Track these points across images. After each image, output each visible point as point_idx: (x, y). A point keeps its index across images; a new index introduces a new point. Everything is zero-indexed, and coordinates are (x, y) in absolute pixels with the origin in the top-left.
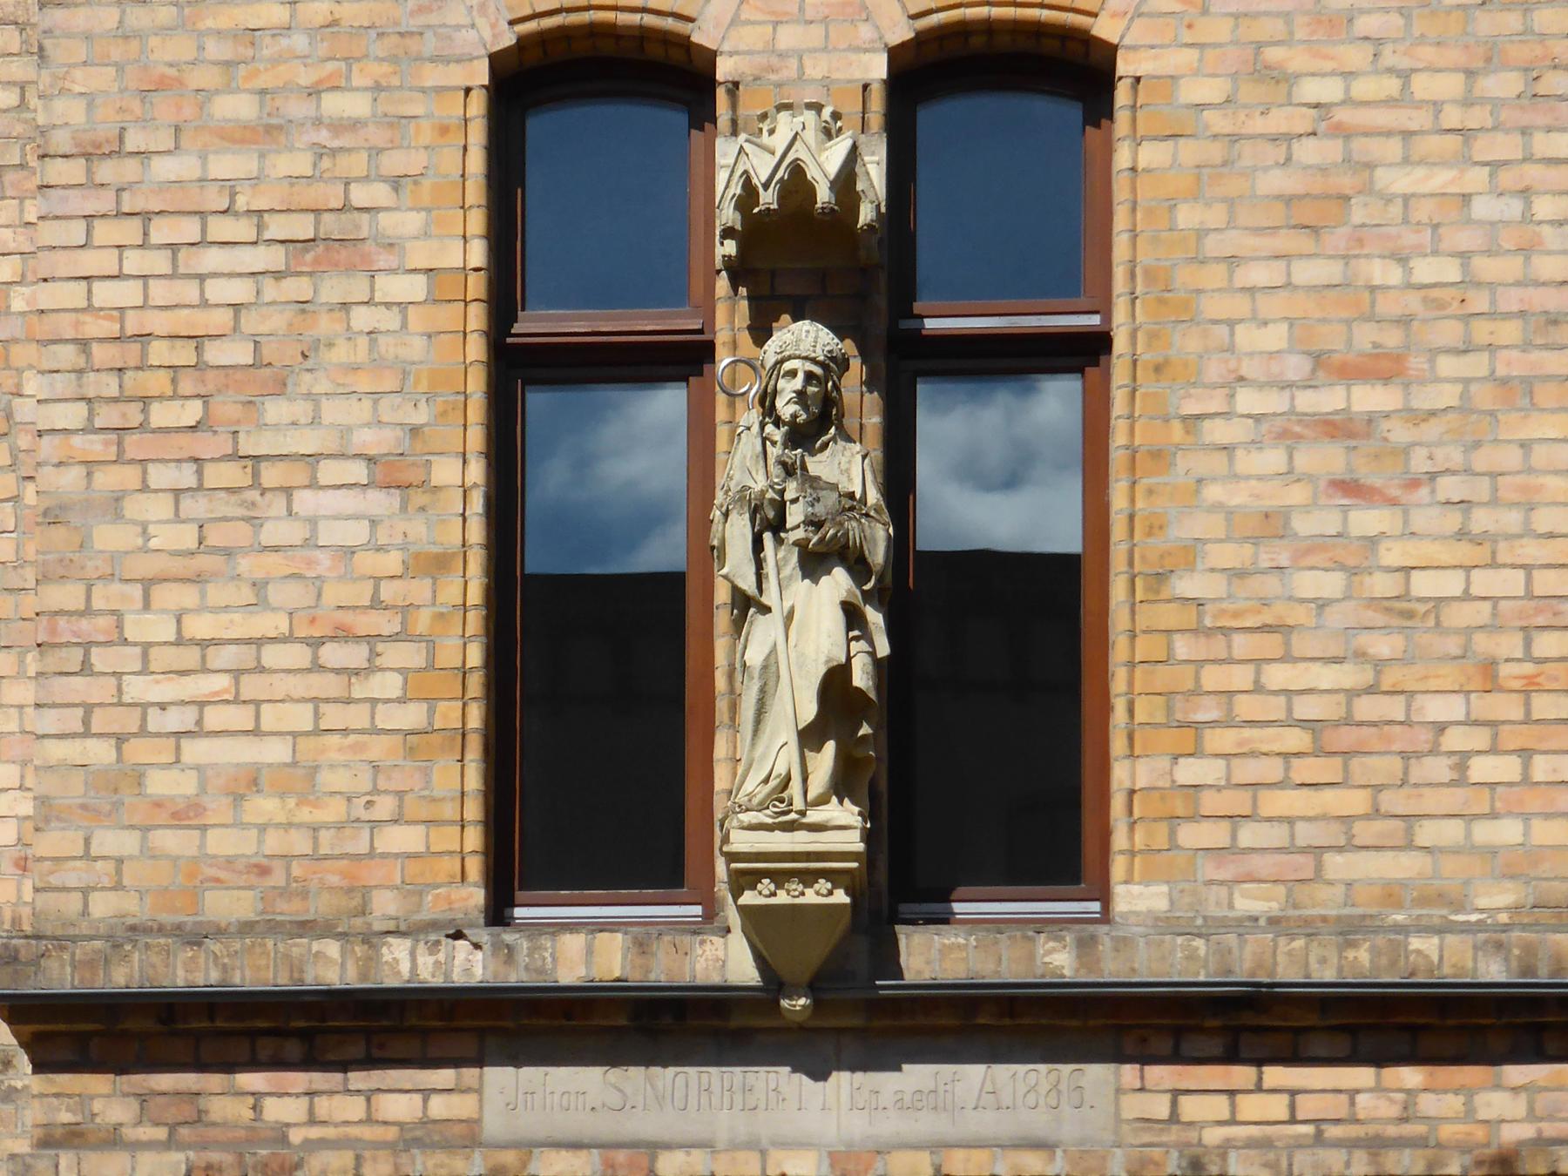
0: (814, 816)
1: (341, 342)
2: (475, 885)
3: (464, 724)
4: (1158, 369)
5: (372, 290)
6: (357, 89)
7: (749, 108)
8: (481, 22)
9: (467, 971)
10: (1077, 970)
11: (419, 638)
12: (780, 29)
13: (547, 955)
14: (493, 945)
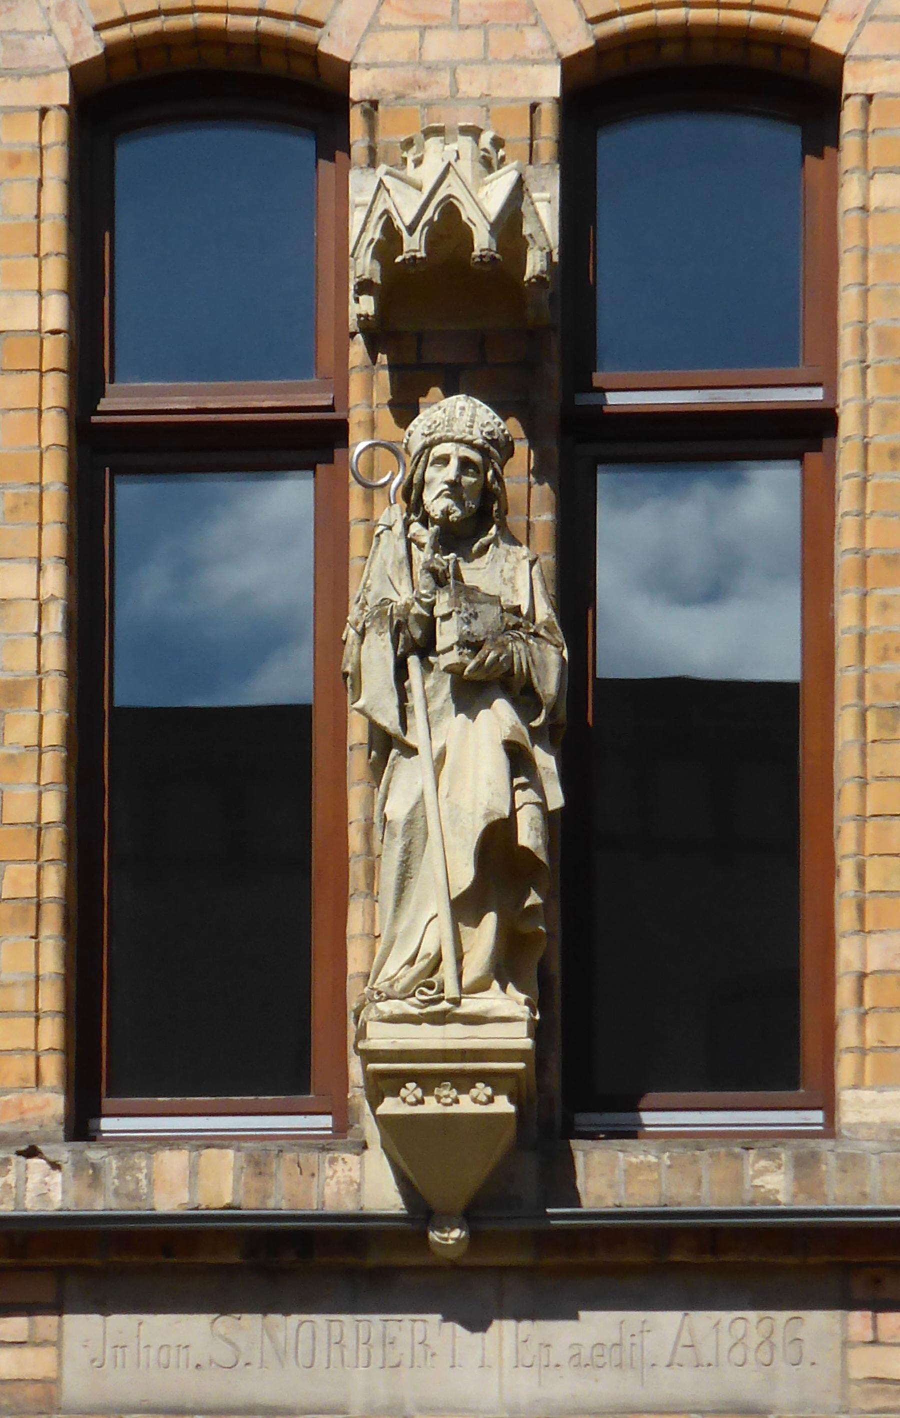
0: (470, 1005)
2: (53, 1090)
8: (60, 28)
10: (795, 1196)
12: (428, 35)
13: (141, 1176)
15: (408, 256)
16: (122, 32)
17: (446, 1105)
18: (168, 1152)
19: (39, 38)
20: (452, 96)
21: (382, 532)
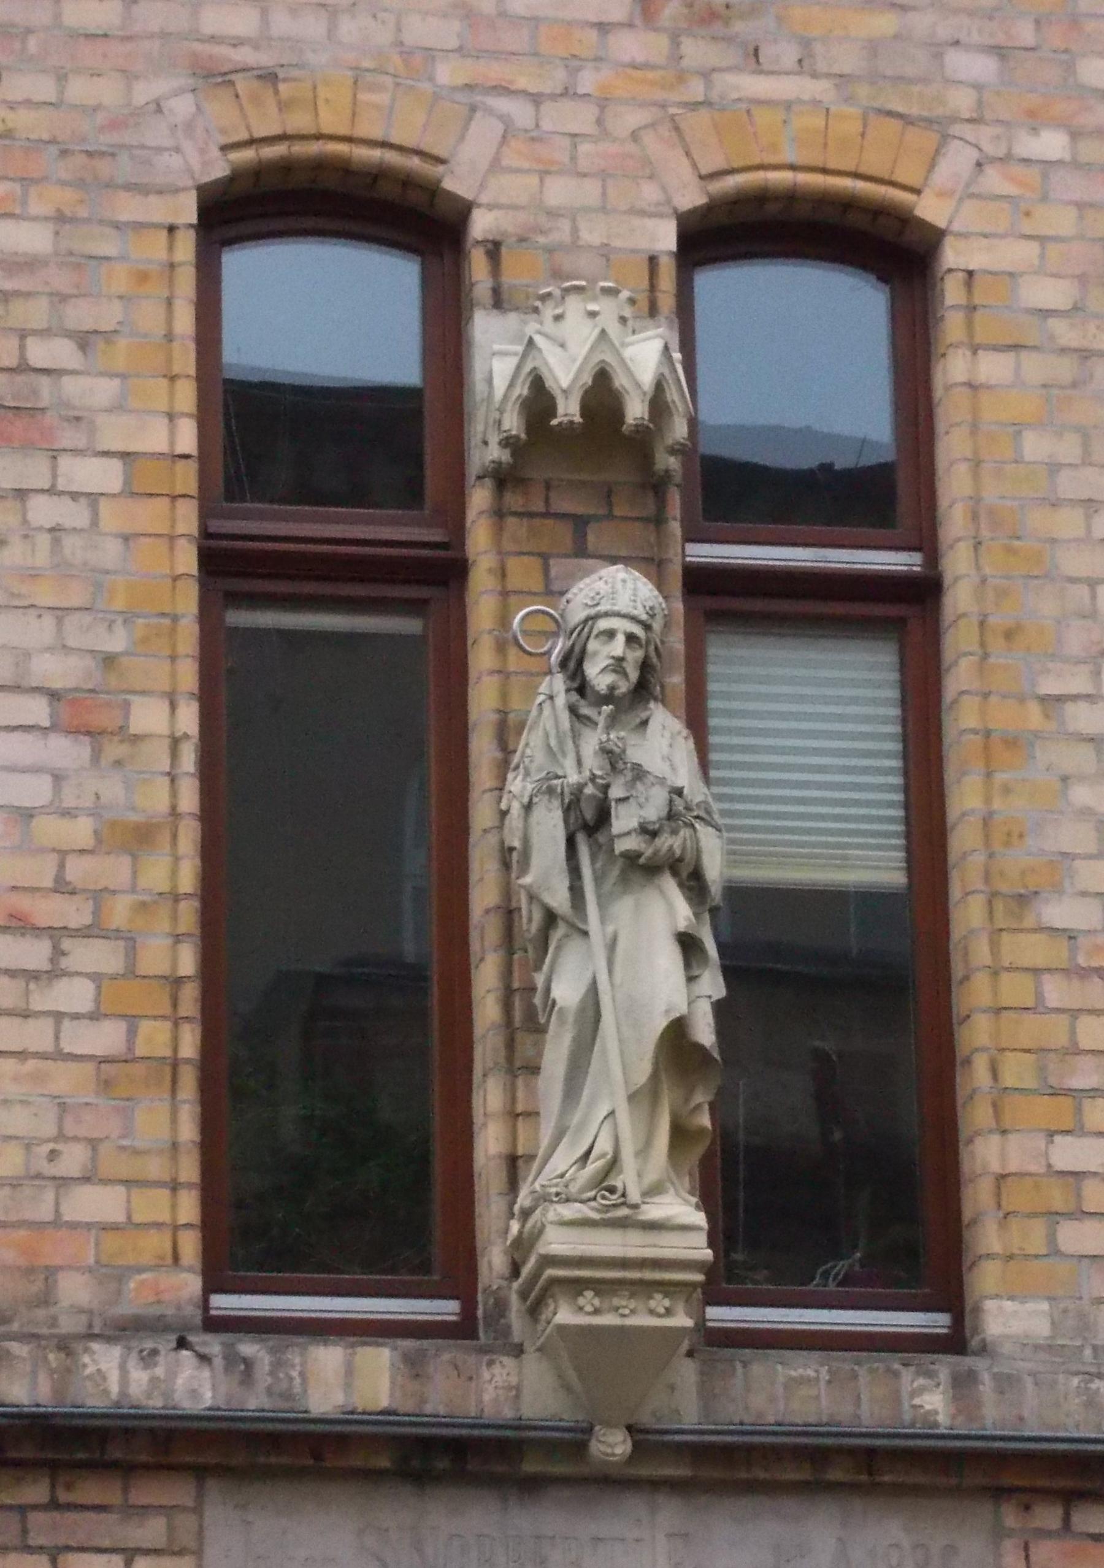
0: (653, 1211)
1: (15, 540)
2: (190, 1269)
3: (175, 1050)
4: (1009, 635)
5: (55, 476)
6: (35, 219)
7: (516, 274)
8: (188, 147)
9: (194, 1393)
10: (954, 1417)
11: (118, 934)
12: (549, 180)
13: (295, 1374)
14: (225, 1358)
15: (565, 419)
16: (247, 155)
17: (624, 1316)
18: (322, 1348)
19: (166, 154)
20: (574, 243)
21: (544, 702)
